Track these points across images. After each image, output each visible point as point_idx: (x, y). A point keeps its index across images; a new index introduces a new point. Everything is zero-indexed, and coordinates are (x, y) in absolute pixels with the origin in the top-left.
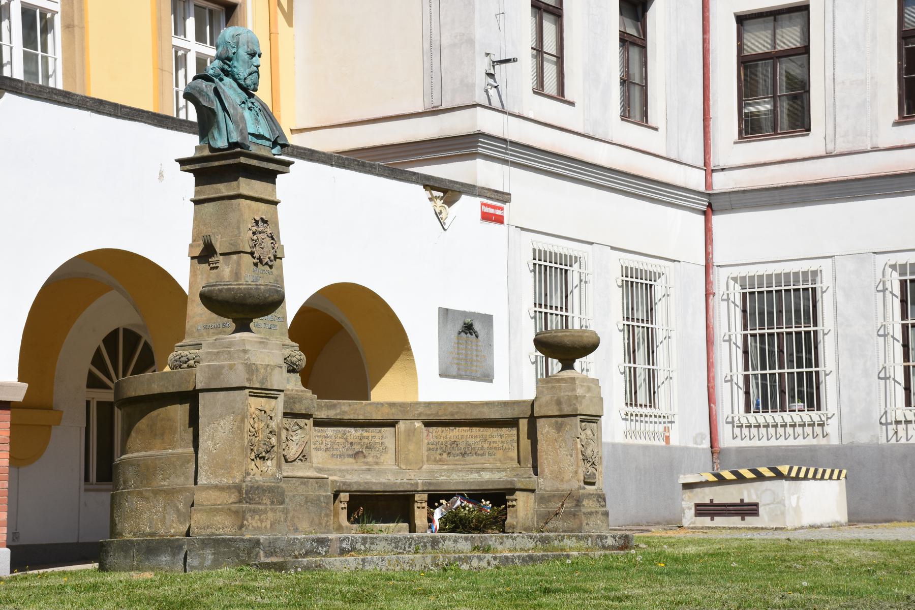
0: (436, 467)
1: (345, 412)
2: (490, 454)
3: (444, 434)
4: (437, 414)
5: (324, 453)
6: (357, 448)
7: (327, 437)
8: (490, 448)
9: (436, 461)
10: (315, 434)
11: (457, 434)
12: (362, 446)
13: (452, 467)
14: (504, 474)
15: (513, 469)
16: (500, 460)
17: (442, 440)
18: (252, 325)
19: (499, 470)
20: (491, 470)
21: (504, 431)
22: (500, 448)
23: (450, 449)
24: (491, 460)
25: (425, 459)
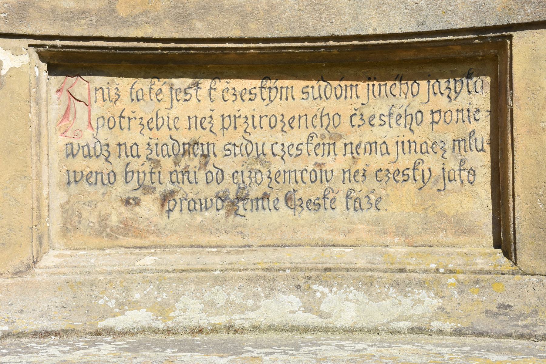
0: (103, 260)
2: (354, 203)
3: (145, 110)
8: (350, 175)
9: (106, 233)
11: (204, 109)
13: (178, 259)
14: (430, 302)
15: (478, 279)
16: (402, 231)
17: (132, 136)
18: (126, 313)
19: (402, 278)
20: (365, 279)
21: (422, 96)
22: (401, 176)
23: (171, 178)
24: (361, 231)
25: (54, 222)
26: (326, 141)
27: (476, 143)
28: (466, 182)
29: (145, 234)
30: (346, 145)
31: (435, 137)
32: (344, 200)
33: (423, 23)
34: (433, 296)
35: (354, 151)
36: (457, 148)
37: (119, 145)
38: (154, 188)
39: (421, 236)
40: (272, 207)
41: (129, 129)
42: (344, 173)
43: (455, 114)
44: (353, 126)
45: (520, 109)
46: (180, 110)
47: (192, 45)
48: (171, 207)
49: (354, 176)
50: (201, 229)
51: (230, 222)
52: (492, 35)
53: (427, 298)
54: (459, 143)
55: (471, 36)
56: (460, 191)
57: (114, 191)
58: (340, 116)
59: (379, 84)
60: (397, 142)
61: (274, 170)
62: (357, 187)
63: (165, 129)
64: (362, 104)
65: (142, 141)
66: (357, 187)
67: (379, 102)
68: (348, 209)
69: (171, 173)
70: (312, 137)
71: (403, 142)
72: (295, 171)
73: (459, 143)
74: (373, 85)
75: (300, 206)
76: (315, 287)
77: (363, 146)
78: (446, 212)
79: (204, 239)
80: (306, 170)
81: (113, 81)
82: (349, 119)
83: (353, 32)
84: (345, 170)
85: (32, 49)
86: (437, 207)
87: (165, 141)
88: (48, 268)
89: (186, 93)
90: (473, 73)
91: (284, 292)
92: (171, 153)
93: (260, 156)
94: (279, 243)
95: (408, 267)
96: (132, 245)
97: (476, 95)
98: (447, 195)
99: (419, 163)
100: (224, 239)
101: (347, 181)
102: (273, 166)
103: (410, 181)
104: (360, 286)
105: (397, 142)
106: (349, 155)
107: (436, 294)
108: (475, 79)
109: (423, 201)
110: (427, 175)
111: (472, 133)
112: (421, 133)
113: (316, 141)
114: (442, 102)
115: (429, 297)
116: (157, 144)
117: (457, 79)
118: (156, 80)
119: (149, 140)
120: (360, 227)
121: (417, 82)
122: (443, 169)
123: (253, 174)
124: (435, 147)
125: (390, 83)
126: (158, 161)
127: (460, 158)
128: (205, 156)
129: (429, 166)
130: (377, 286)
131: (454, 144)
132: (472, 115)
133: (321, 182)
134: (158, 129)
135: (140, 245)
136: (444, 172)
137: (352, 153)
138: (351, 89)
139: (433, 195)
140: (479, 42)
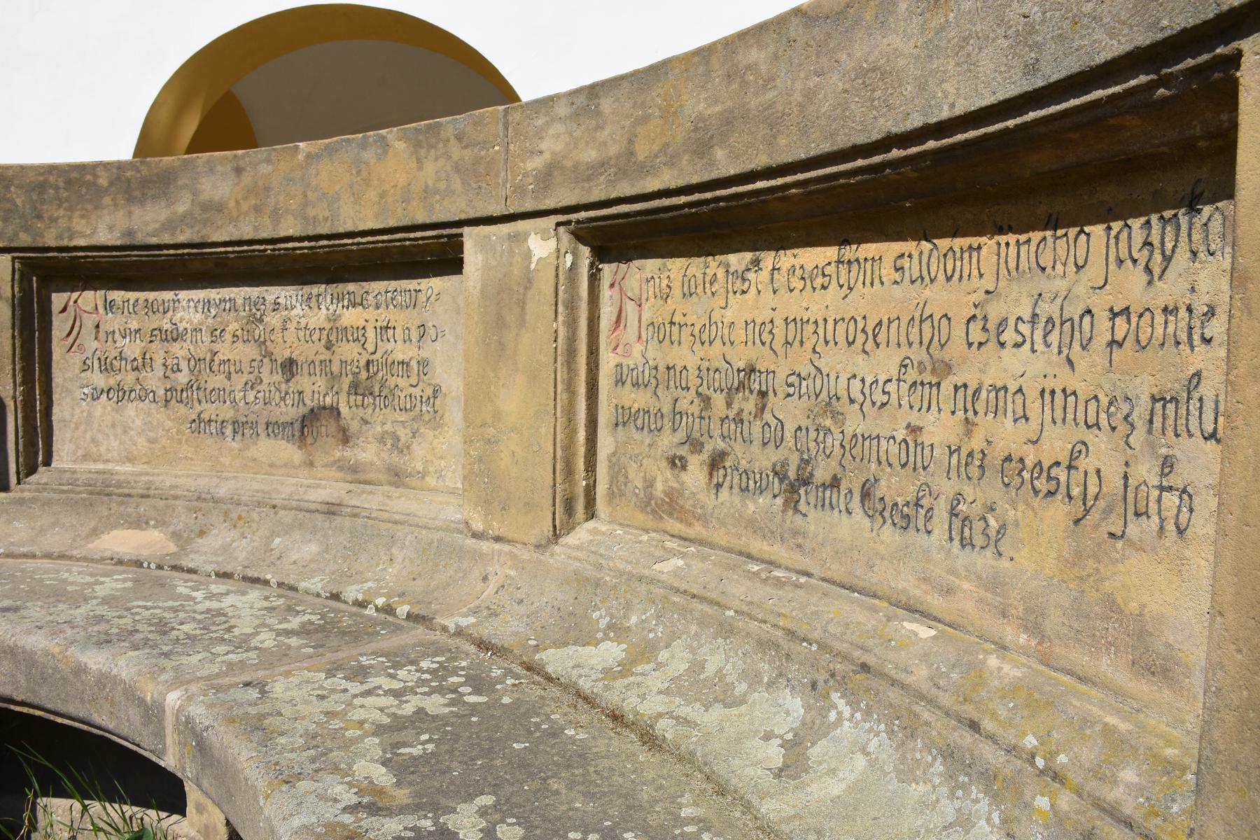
1: (218, 207)
2: (963, 528)
3: (695, 312)
4: (627, 163)
5: (158, 414)
6: (313, 388)
7: (175, 336)
10: (112, 322)
12: (334, 378)
17: (686, 356)
22: (1045, 480)
26: (927, 377)
27: (1201, 413)
28: (1170, 527)
29: (691, 519)
30: (956, 388)
31: (1114, 385)
32: (946, 515)
33: (1031, 69)
34: (997, 821)
35: (969, 406)
36: (1157, 423)
37: (668, 368)
38: (702, 444)
39: (1067, 646)
40: (842, 507)
41: (680, 343)
42: (951, 454)
43: (1159, 319)
44: (970, 345)
45: (1250, 313)
46: (738, 310)
47: (719, 193)
48: (721, 480)
49: (966, 465)
50: (752, 525)
51: (788, 522)
52: (1190, 62)
53: (983, 823)
54: (1164, 407)
55: (1143, 79)
56: (1154, 550)
57: (660, 444)
58: (949, 319)
59: (1018, 241)
60: (1043, 391)
61: (849, 431)
62: (969, 492)
63: (718, 342)
64: (988, 292)
65: (692, 361)
66: (969, 492)
67: (1015, 286)
68: (951, 539)
69: (722, 421)
70: (905, 366)
71: (1053, 392)
72: (878, 436)
73: (1164, 407)
74: (1007, 244)
75: (881, 514)
76: (835, 696)
77: (984, 394)
78: (1119, 600)
79: (758, 546)
80: (893, 438)
81: (665, 266)
82: (964, 327)
83: (915, 122)
84: (953, 448)
85: (562, 229)
86: (1102, 580)
87: (717, 365)
88: (570, 547)
89: (744, 280)
90: (1202, 194)
91: (793, 688)
92: (724, 385)
93: (830, 406)
94: (847, 581)
95: (988, 725)
96: (676, 532)
97: (79, 309)
98: (1127, 553)
99: (1080, 452)
100: (778, 551)
101: (953, 474)
102: (848, 423)
103: (1060, 497)
104: (896, 728)
105: (1043, 391)
106: (960, 414)
107: (1004, 821)
108: (1207, 210)
109: (1078, 556)
110: (1093, 490)
111: (1195, 381)
112: (1090, 372)
113: (912, 375)
114: (1131, 286)
115: (988, 820)
116: (708, 370)
117: (1168, 214)
118: (711, 258)
119: (699, 362)
120: (966, 585)
121: (1087, 229)
122: (1126, 477)
123: (822, 434)
124: (1112, 413)
125: (1036, 236)
126: (709, 399)
127: (1163, 451)
128: (763, 394)
129: (1098, 464)
130: (919, 743)
131: (1152, 410)
132: (1198, 324)
133: (915, 469)
134: (711, 343)
135: (684, 535)
136: (1126, 487)
137: (966, 411)
138: (970, 257)
139: (1099, 545)
140: (1167, 93)
